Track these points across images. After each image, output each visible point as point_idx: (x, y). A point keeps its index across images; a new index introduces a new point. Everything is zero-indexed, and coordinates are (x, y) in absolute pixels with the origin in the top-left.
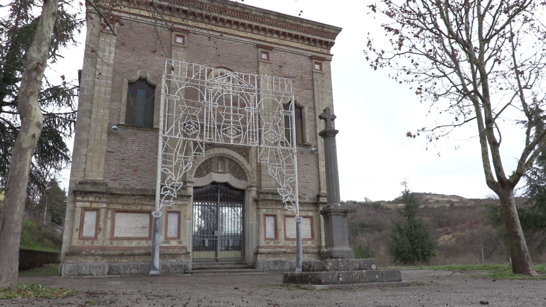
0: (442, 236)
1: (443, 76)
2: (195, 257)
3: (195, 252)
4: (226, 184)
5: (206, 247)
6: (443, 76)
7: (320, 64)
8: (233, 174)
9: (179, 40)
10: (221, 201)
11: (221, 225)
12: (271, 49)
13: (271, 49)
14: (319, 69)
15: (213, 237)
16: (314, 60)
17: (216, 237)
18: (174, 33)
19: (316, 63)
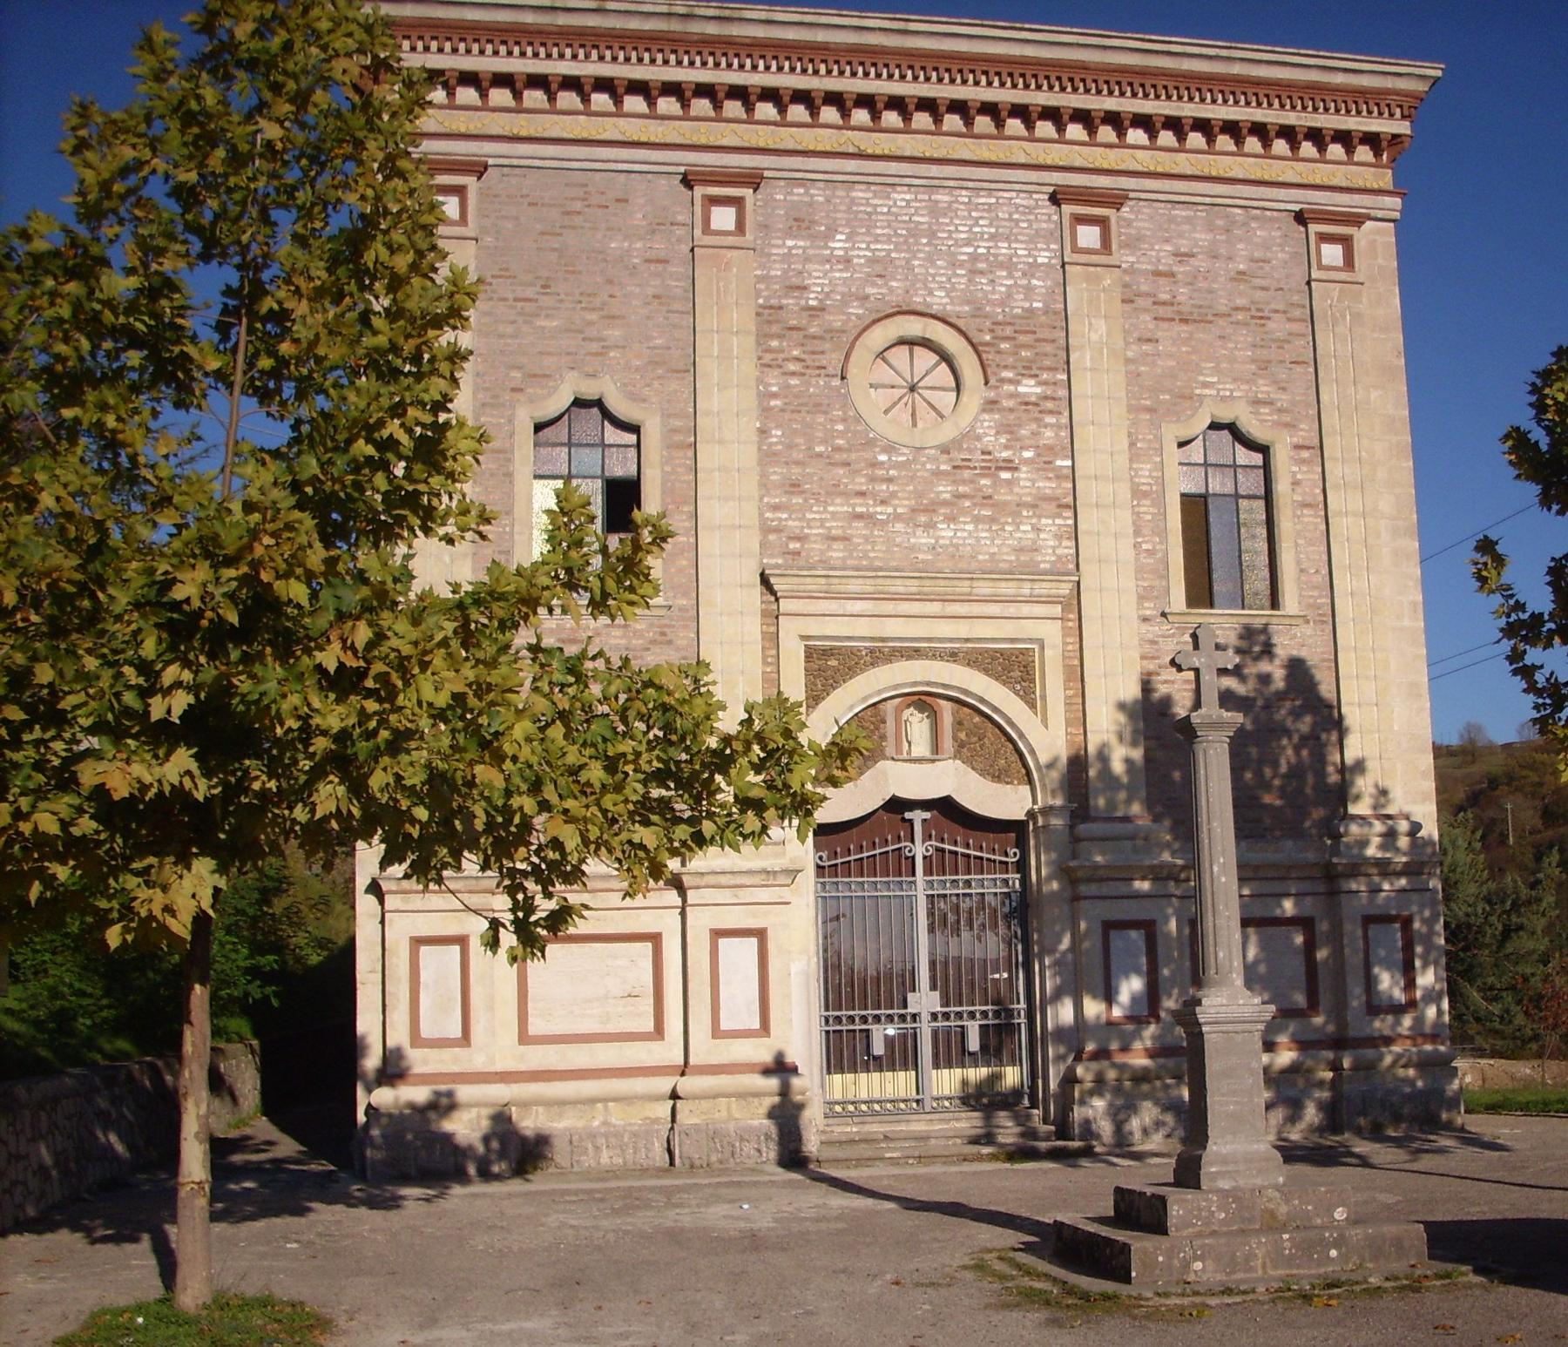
0: (556, 1212)
1: (222, 424)
2: (838, 1096)
3: (837, 1078)
4: (946, 808)
5: (876, 1058)
6: (222, 424)
7: (1346, 241)
8: (969, 762)
9: (723, 218)
10: (928, 871)
11: (1211, 924)
12: (1116, 200)
13: (1116, 200)
14: (1340, 262)
15: (903, 1018)
16: (1314, 228)
17: (914, 1017)
18: (699, 191)
19: (1324, 238)
